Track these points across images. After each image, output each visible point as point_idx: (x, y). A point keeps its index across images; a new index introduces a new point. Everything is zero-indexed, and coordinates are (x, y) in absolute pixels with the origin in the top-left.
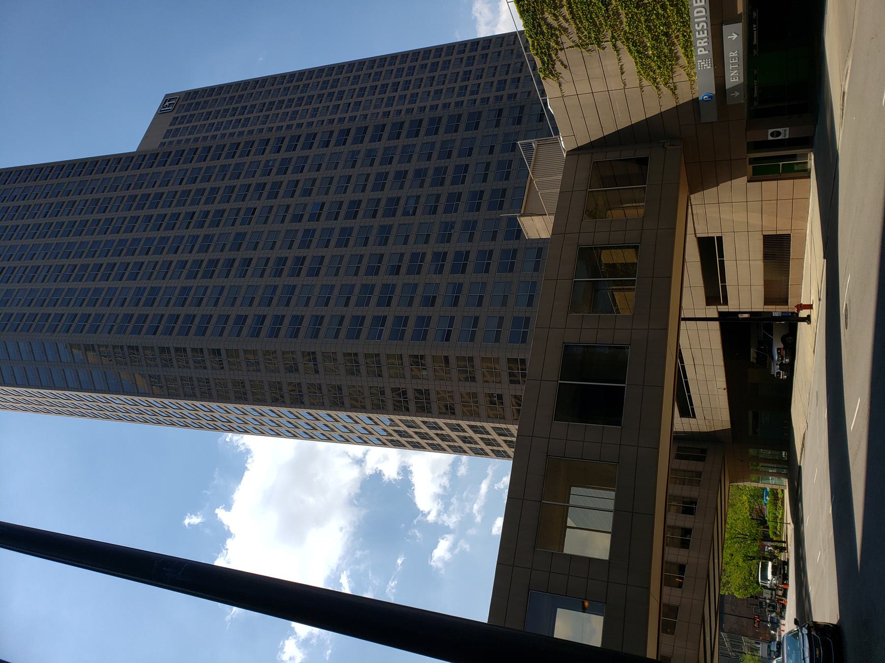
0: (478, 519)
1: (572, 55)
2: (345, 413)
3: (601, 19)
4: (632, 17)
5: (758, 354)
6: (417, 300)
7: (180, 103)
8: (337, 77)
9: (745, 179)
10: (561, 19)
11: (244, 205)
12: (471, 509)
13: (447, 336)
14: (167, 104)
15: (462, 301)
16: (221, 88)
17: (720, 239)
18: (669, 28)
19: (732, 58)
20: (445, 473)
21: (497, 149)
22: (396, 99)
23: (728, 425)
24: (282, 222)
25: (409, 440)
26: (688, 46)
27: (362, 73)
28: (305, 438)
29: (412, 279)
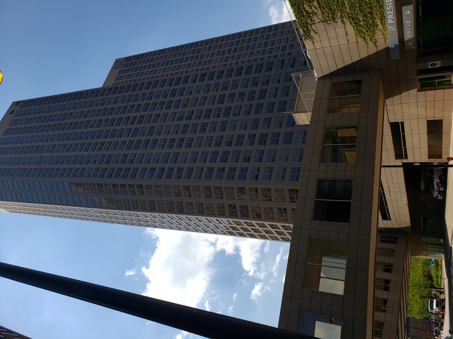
0: (275, 275)
1: (319, 27)
2: (205, 217)
3: (335, 6)
4: (352, 5)
5: (425, 185)
6: (241, 159)
7: (123, 63)
8: (200, 47)
9: (416, 90)
10: (313, 8)
11: (154, 113)
12: (272, 269)
13: (257, 178)
14: (117, 64)
15: (264, 159)
16: (143, 55)
17: (402, 123)
18: (372, 9)
19: (408, 24)
20: (258, 251)
21: (282, 81)
22: (230, 57)
23: (409, 224)
24: (173, 121)
25: (238, 231)
26: (383, 19)
27: (213, 45)
28: (185, 230)
29: (238, 148)
